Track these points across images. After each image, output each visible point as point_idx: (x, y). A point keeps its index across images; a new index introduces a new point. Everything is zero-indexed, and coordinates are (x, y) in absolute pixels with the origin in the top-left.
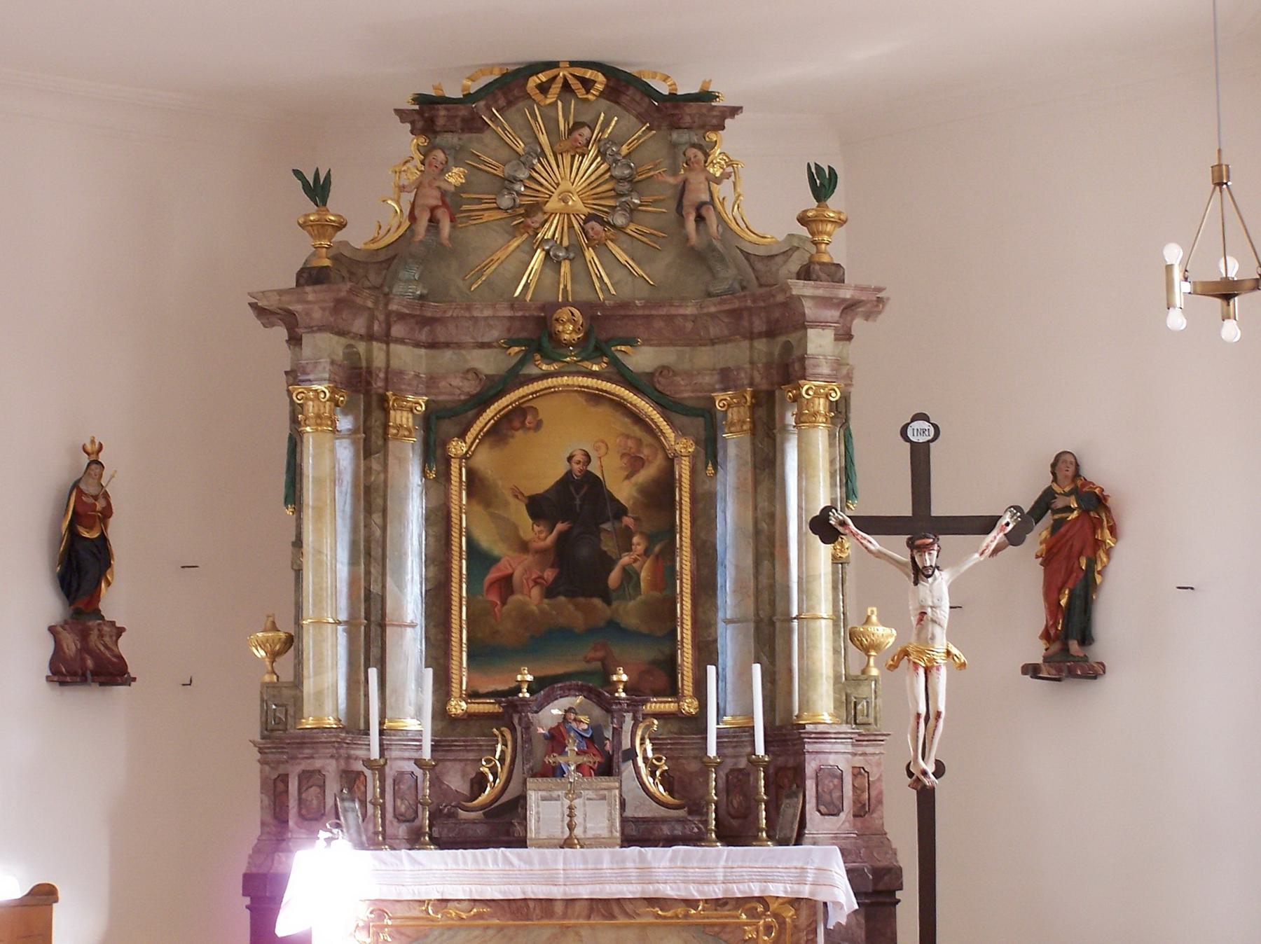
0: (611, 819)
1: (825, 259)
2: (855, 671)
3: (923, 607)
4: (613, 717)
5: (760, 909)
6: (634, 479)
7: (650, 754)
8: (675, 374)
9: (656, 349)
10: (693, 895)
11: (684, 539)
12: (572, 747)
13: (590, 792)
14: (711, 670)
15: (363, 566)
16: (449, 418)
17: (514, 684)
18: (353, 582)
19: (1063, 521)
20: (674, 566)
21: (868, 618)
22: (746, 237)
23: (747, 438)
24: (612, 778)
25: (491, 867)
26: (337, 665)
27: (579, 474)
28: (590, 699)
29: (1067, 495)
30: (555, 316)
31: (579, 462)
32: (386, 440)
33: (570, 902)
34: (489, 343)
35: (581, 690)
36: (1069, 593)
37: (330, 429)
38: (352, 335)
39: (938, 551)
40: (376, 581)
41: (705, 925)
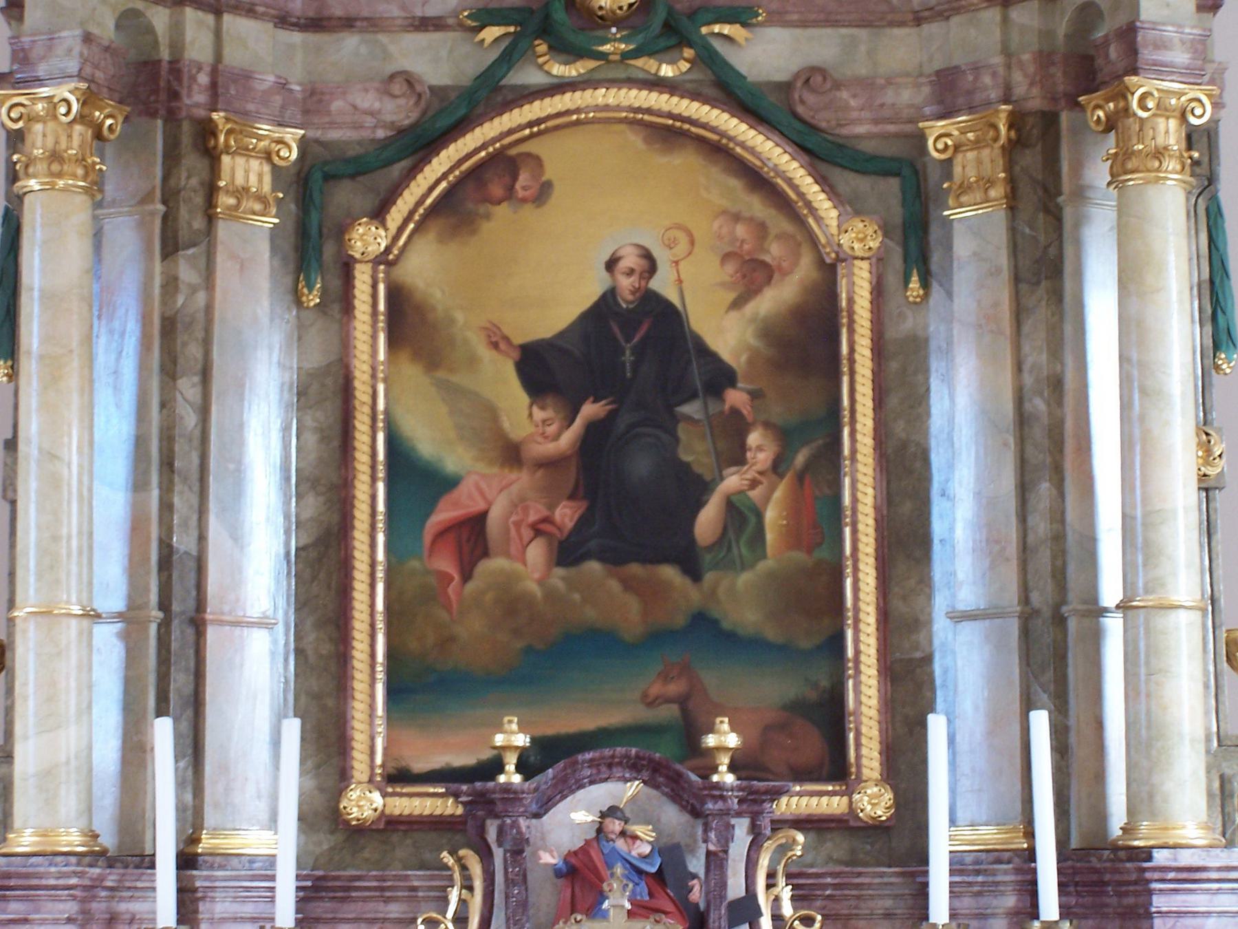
6: (750, 308)
7: (787, 910)
8: (838, 85)
15: (155, 493)
16: (353, 177)
17: (486, 754)
18: (137, 527)
20: (838, 497)
23: (1000, 217)
26: (90, 707)
27: (630, 298)
28: (656, 787)
31: (631, 272)
32: (211, 219)
34: (440, 18)
35: (635, 767)
40: (185, 524)
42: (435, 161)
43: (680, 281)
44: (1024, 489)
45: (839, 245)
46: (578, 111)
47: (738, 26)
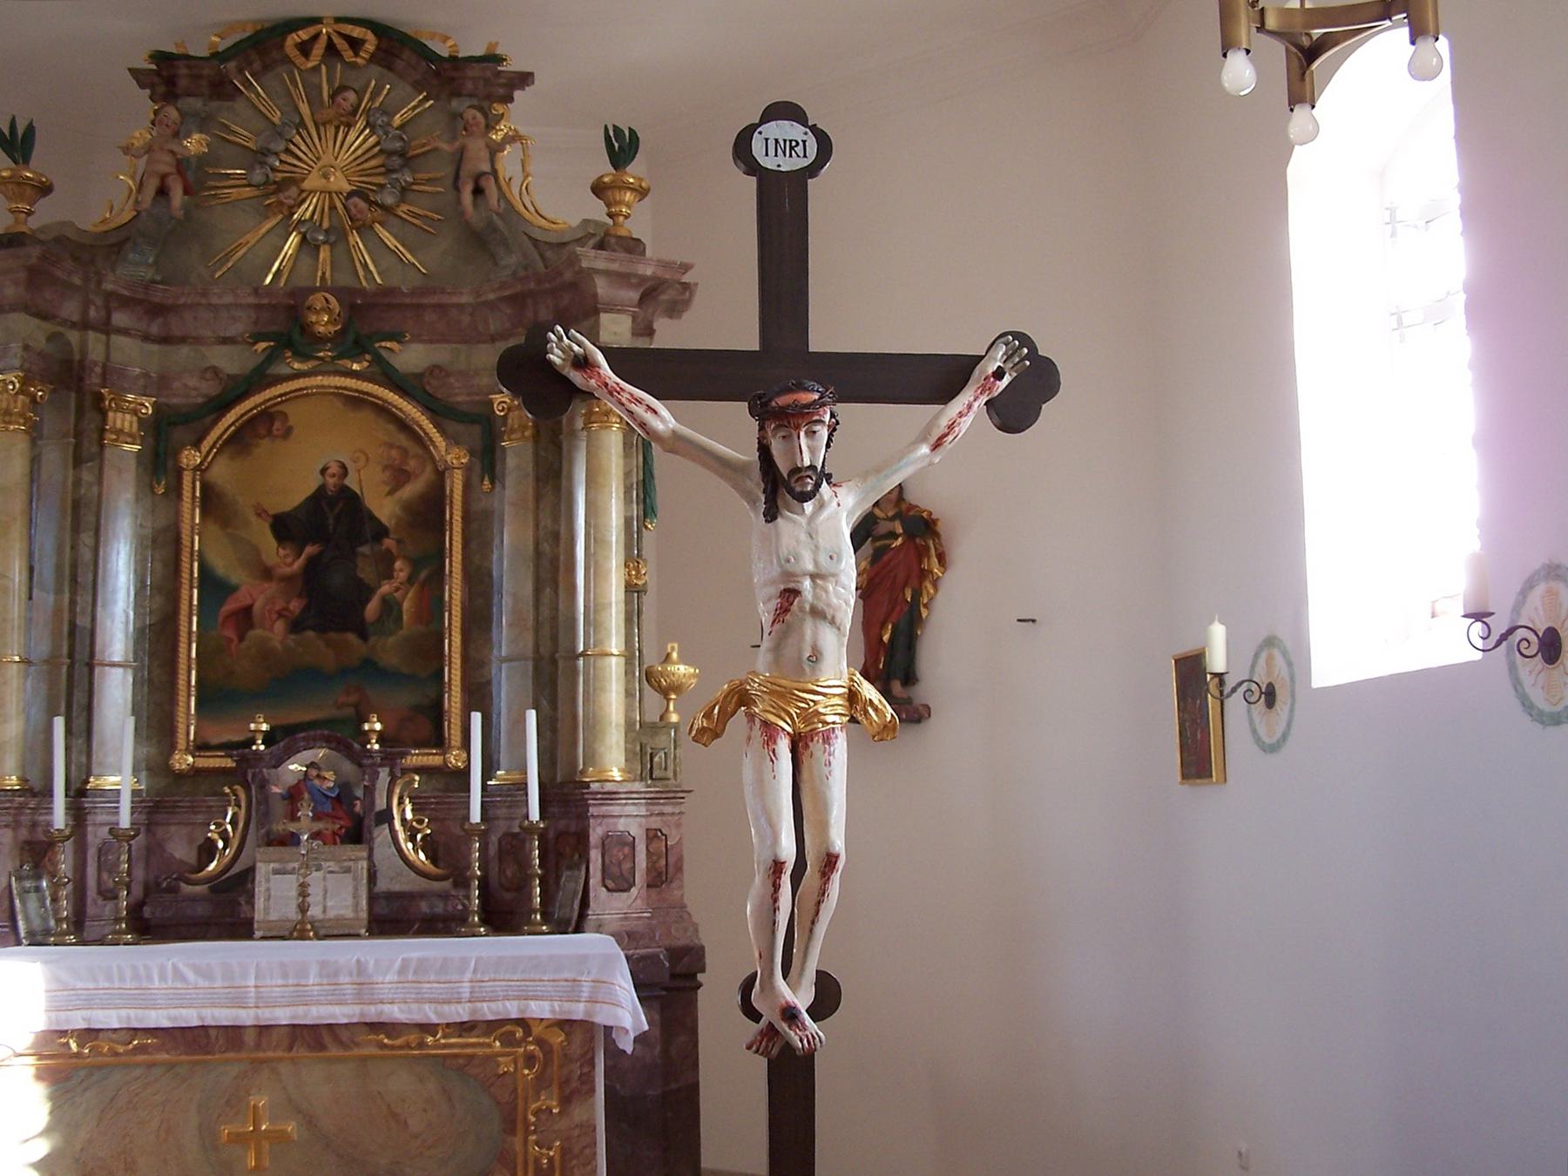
0: (355, 896)
1: (623, 233)
2: (653, 716)
3: (788, 575)
4: (364, 773)
5: (519, 1034)
6: (398, 494)
7: (409, 815)
9: (428, 346)
10: (428, 1018)
11: (455, 565)
12: (306, 812)
13: (331, 863)
14: (476, 718)
19: (887, 548)
21: (668, 656)
22: (535, 222)
23: (530, 446)
24: (359, 846)
25: (157, 984)
27: (333, 489)
29: (892, 519)
30: (307, 304)
31: (334, 475)
32: (102, 446)
33: (264, 1030)
35: (329, 741)
36: (892, 627)
37: (23, 428)
38: (59, 320)
39: (832, 430)
41: (445, 1056)
42: (228, 416)
43: (360, 481)
44: (537, 591)
45: (446, 462)
46: (306, 388)
47: (395, 343)
